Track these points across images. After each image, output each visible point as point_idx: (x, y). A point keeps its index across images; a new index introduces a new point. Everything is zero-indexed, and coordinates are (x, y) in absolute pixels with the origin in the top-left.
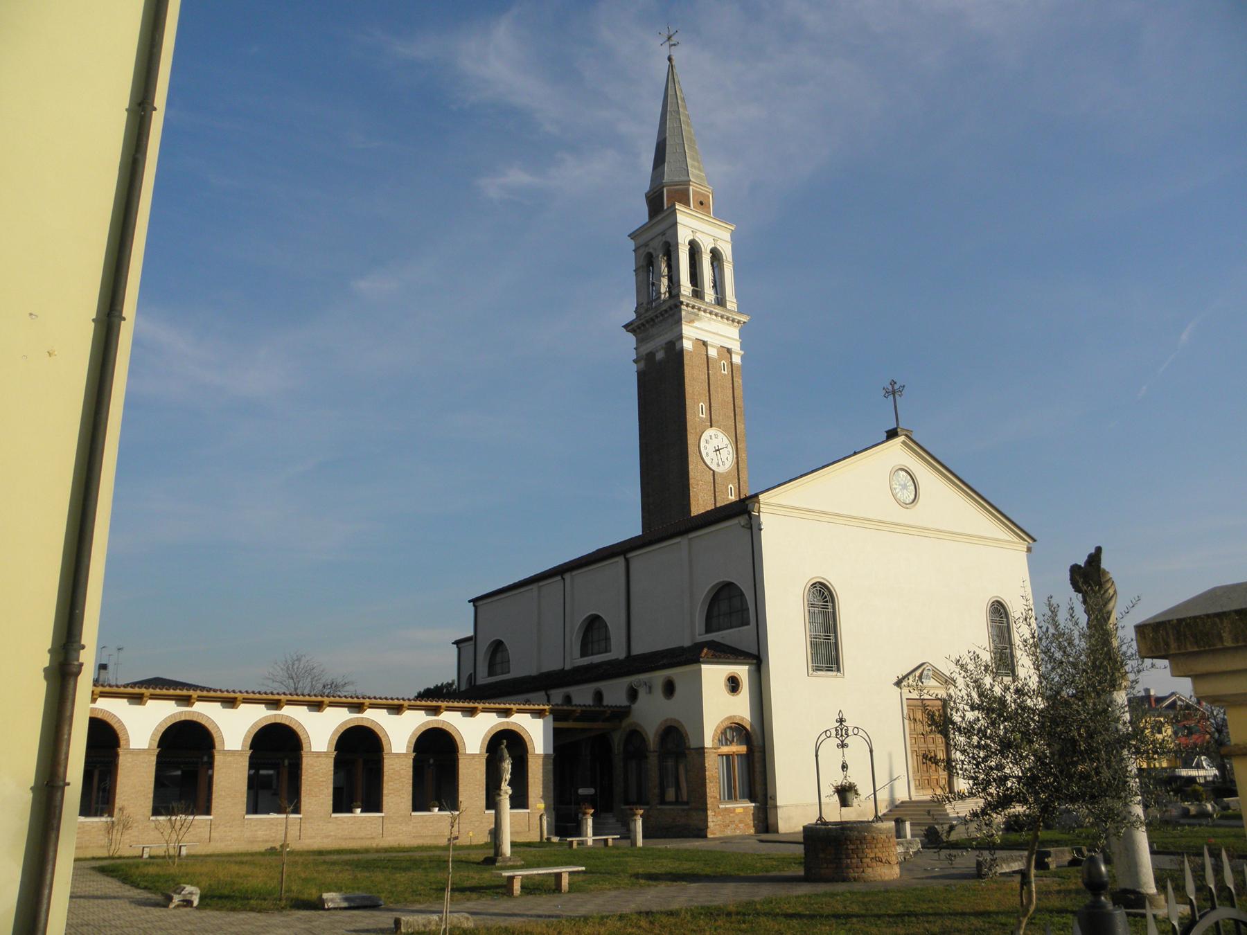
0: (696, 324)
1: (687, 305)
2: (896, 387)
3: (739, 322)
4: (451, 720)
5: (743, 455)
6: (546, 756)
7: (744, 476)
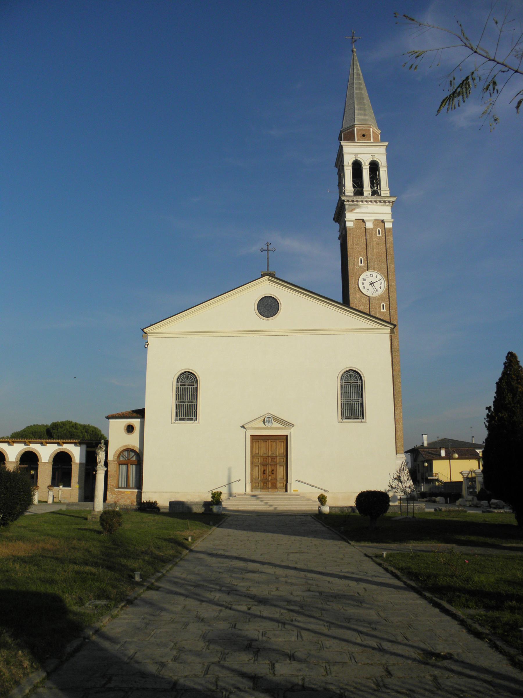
0: (357, 211)
1: (348, 201)
2: (270, 247)
3: (389, 202)
4: (36, 447)
5: (392, 283)
6: (80, 464)
7: (393, 296)
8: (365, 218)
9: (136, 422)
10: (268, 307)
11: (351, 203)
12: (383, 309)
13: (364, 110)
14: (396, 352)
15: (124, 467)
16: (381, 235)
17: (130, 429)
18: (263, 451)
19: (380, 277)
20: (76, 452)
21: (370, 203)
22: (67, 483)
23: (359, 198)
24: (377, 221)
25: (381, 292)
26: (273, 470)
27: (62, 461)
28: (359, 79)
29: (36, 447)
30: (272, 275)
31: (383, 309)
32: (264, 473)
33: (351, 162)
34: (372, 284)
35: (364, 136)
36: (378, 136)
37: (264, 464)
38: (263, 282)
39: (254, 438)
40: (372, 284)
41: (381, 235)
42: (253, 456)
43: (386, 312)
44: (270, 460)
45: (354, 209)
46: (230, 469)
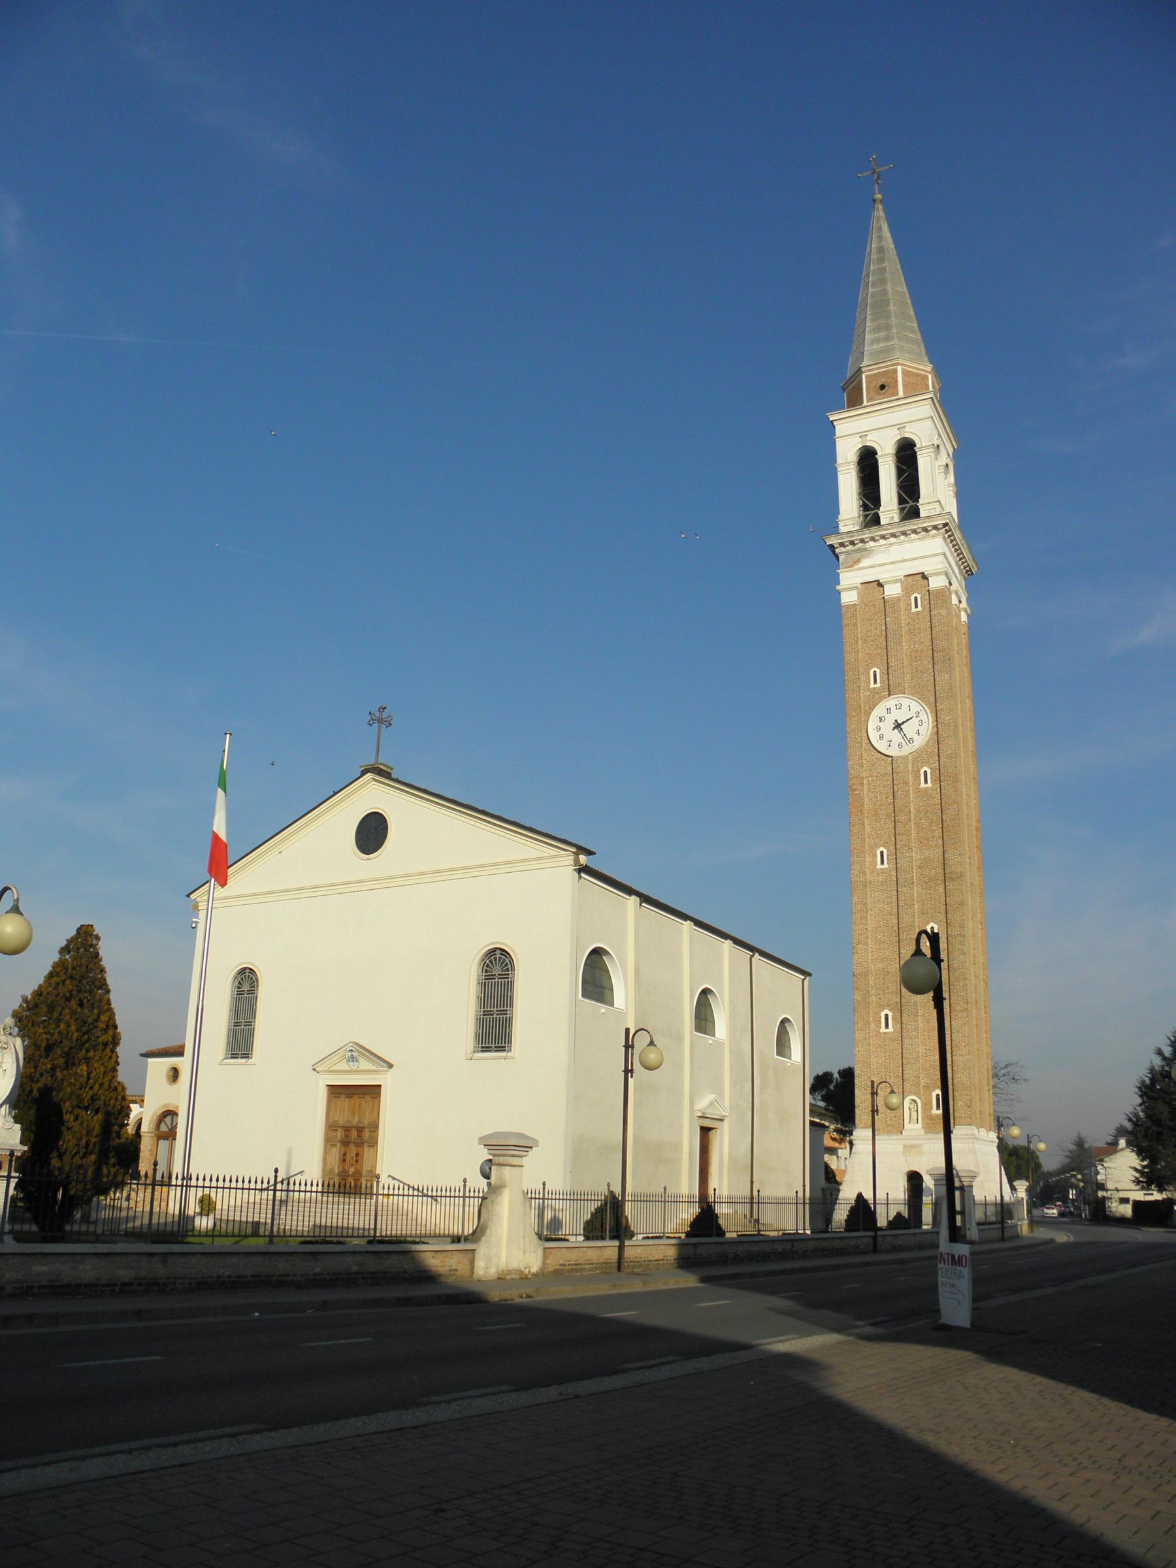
0: (865, 563)
1: (842, 545)
3: (935, 527)
8: (926, 570)
10: (372, 834)
11: (850, 547)
12: (926, 781)
14: (953, 880)
16: (920, 608)
17: (175, 1074)
18: (342, 1118)
19: (919, 708)
21: (892, 540)
23: (875, 532)
24: (910, 579)
25: (919, 742)
26: (357, 1155)
28: (881, 260)
30: (383, 773)
31: (926, 781)
32: (344, 1160)
34: (898, 726)
35: (883, 387)
36: (925, 378)
37: (345, 1143)
38: (364, 785)
39: (336, 1091)
40: (898, 726)
41: (920, 608)
42: (331, 1127)
43: (931, 789)
44: (354, 1134)
45: (858, 561)
46: (290, 1152)
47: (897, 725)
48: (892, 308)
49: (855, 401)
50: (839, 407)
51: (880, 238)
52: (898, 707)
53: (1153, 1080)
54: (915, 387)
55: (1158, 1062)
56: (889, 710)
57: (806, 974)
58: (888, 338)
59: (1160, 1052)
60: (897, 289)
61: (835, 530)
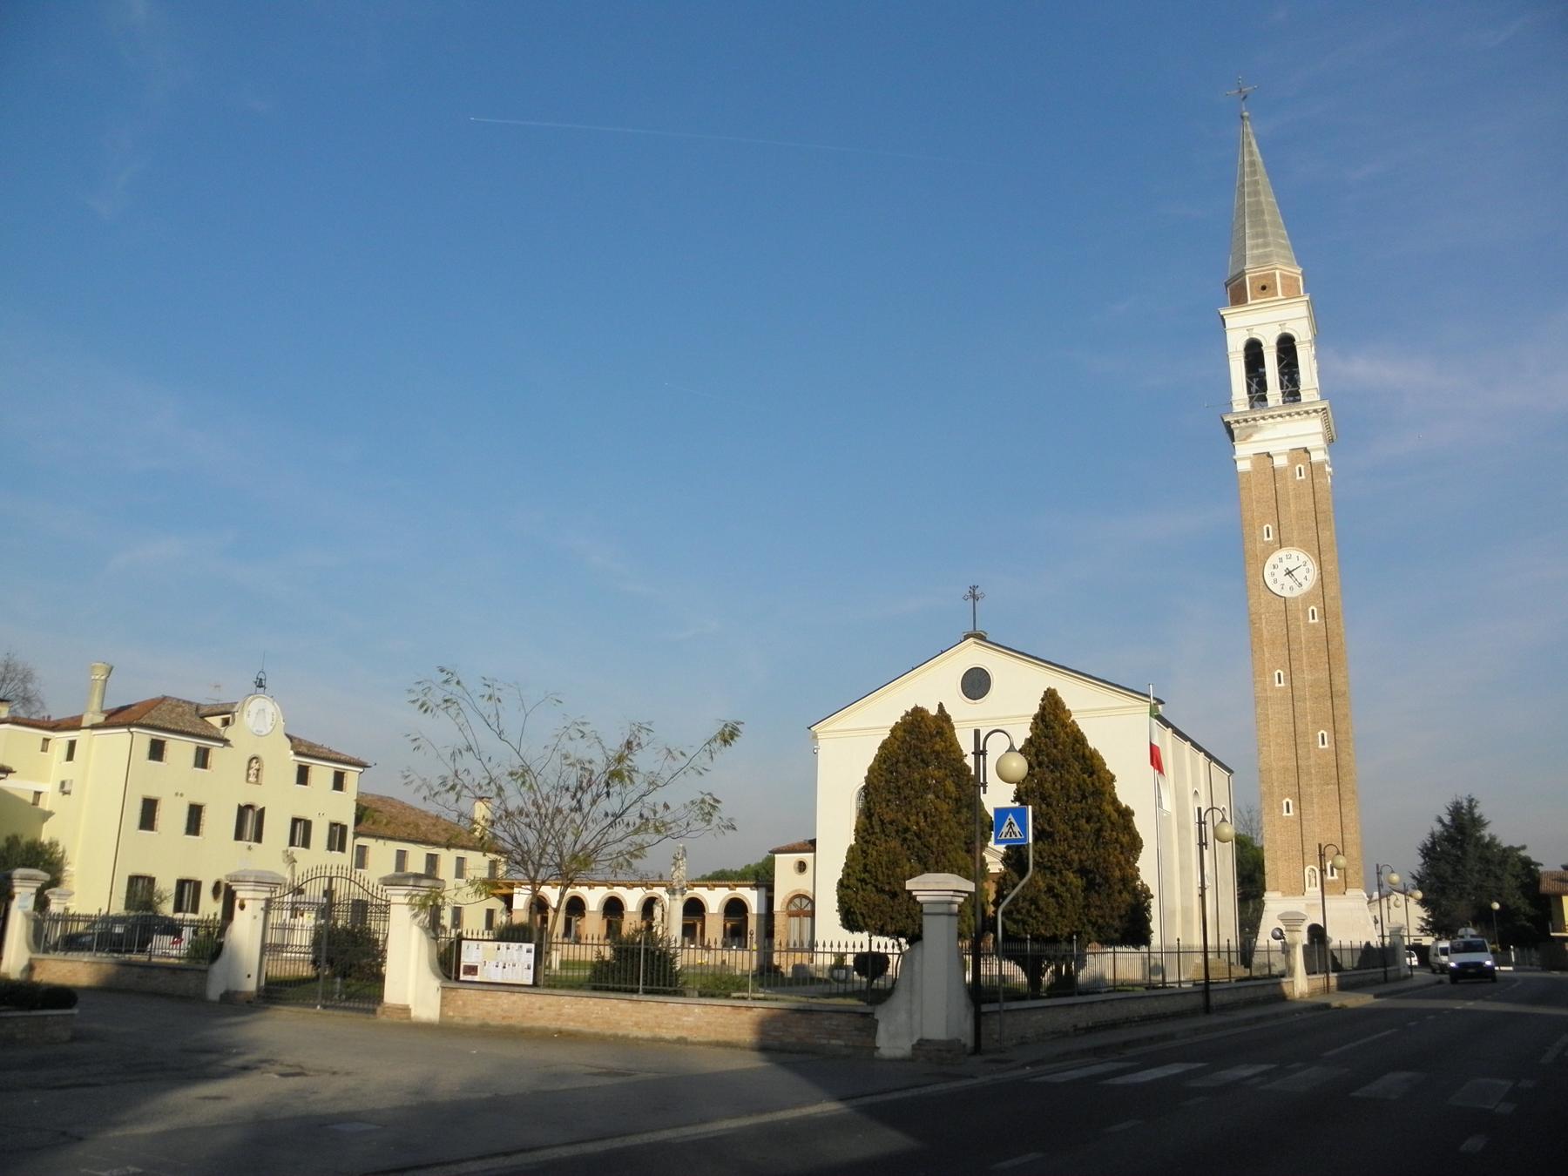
0: (1256, 437)
4: (619, 891)
5: (1329, 567)
7: (1332, 590)
9: (807, 857)
13: (1264, 235)
15: (796, 920)
17: (802, 867)
20: (752, 897)
22: (342, 848)
25: (1307, 586)
27: (735, 908)
28: (1254, 173)
29: (619, 891)
30: (981, 637)
33: (1241, 347)
34: (1289, 573)
35: (1264, 288)
40: (1289, 573)
47: (1290, 572)
48: (1267, 218)
49: (1239, 298)
50: (1225, 305)
51: (1251, 153)
52: (1289, 557)
53: (1434, 843)
54: (1291, 291)
55: (1438, 828)
56: (1281, 560)
57: (1230, 771)
58: (1266, 245)
59: (1440, 820)
60: (1268, 199)
61: (1230, 411)
